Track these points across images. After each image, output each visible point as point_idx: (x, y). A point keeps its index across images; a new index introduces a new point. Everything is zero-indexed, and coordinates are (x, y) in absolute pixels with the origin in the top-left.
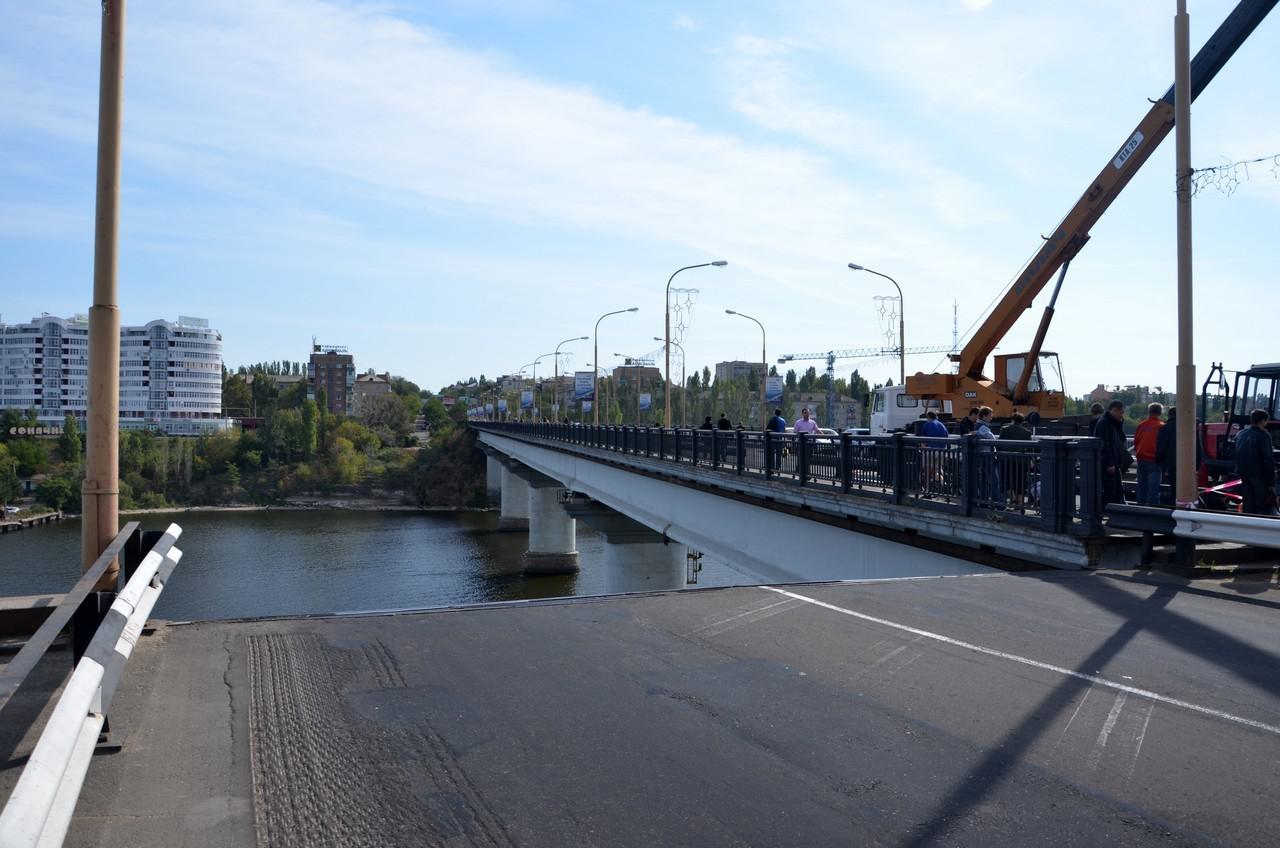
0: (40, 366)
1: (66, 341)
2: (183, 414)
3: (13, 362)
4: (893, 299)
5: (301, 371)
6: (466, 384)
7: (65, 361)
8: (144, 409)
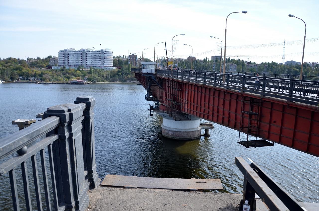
0: (82, 58)
1: (86, 53)
2: (107, 66)
3: (78, 57)
4: (220, 43)
5: (126, 58)
7: (86, 57)
8: (100, 65)
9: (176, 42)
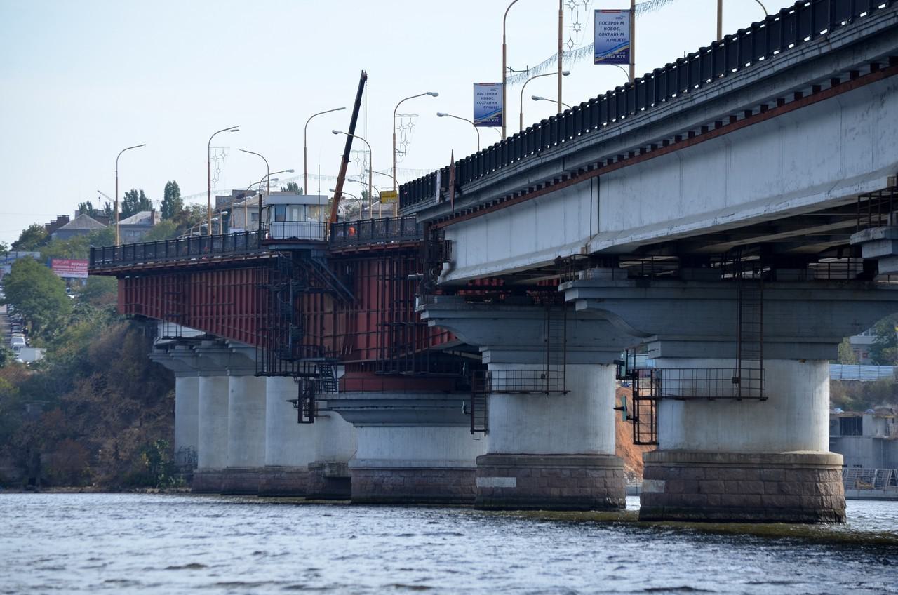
6: (108, 216)
9: (219, 152)
